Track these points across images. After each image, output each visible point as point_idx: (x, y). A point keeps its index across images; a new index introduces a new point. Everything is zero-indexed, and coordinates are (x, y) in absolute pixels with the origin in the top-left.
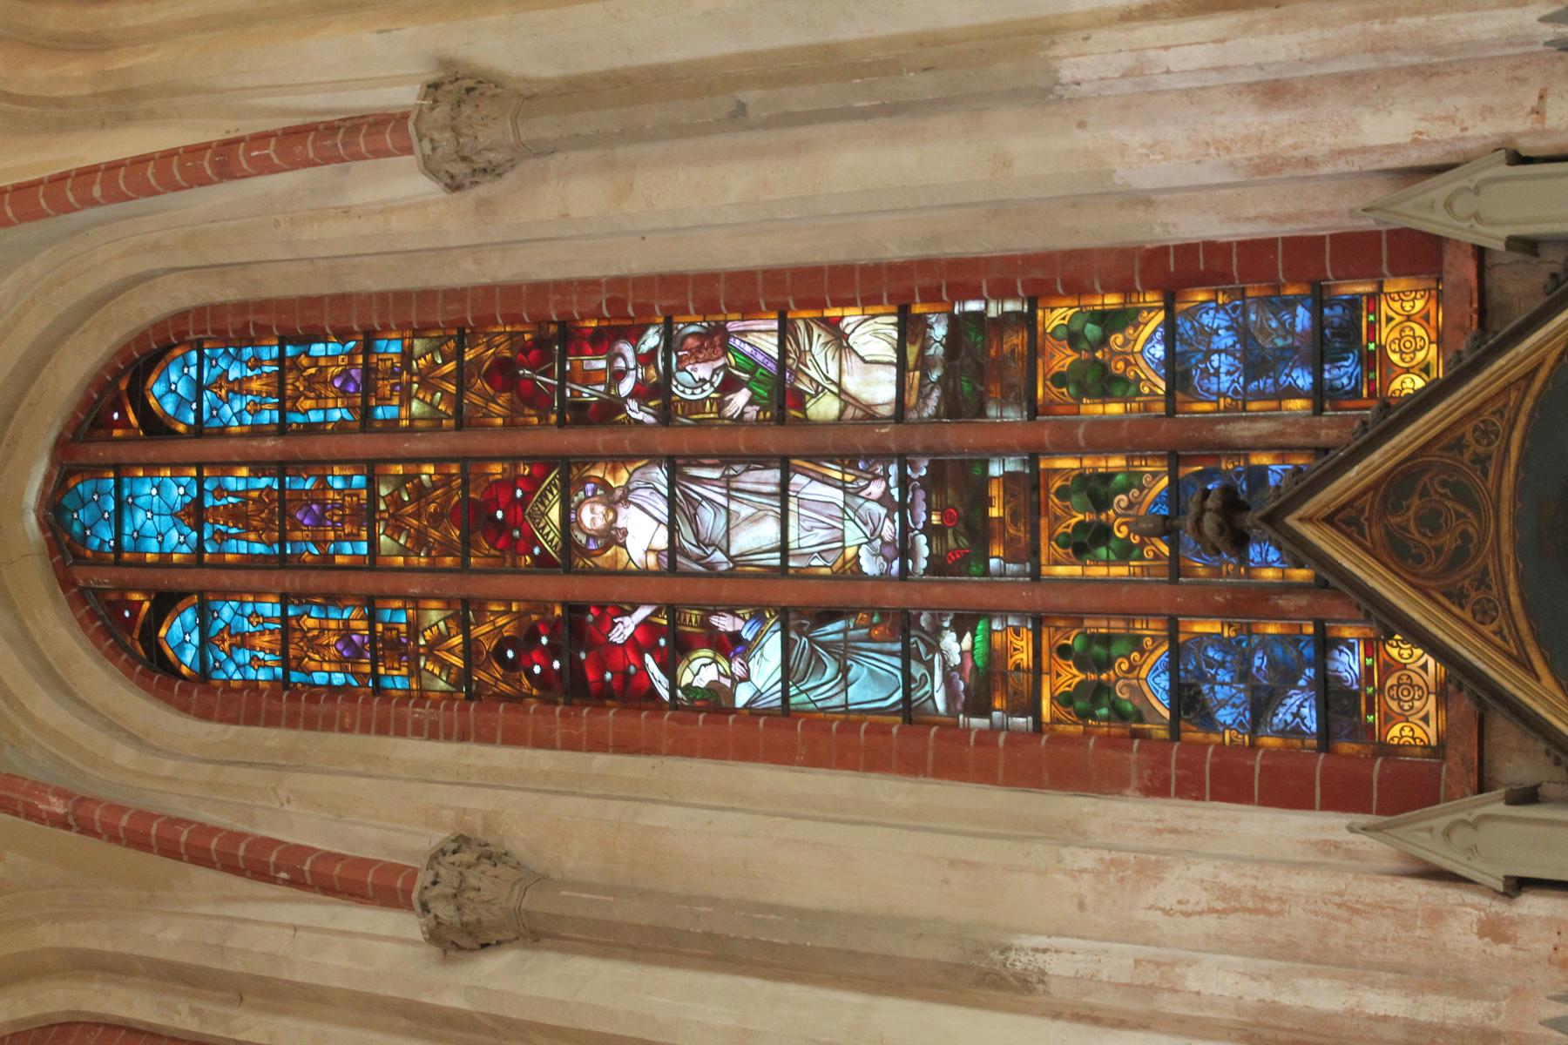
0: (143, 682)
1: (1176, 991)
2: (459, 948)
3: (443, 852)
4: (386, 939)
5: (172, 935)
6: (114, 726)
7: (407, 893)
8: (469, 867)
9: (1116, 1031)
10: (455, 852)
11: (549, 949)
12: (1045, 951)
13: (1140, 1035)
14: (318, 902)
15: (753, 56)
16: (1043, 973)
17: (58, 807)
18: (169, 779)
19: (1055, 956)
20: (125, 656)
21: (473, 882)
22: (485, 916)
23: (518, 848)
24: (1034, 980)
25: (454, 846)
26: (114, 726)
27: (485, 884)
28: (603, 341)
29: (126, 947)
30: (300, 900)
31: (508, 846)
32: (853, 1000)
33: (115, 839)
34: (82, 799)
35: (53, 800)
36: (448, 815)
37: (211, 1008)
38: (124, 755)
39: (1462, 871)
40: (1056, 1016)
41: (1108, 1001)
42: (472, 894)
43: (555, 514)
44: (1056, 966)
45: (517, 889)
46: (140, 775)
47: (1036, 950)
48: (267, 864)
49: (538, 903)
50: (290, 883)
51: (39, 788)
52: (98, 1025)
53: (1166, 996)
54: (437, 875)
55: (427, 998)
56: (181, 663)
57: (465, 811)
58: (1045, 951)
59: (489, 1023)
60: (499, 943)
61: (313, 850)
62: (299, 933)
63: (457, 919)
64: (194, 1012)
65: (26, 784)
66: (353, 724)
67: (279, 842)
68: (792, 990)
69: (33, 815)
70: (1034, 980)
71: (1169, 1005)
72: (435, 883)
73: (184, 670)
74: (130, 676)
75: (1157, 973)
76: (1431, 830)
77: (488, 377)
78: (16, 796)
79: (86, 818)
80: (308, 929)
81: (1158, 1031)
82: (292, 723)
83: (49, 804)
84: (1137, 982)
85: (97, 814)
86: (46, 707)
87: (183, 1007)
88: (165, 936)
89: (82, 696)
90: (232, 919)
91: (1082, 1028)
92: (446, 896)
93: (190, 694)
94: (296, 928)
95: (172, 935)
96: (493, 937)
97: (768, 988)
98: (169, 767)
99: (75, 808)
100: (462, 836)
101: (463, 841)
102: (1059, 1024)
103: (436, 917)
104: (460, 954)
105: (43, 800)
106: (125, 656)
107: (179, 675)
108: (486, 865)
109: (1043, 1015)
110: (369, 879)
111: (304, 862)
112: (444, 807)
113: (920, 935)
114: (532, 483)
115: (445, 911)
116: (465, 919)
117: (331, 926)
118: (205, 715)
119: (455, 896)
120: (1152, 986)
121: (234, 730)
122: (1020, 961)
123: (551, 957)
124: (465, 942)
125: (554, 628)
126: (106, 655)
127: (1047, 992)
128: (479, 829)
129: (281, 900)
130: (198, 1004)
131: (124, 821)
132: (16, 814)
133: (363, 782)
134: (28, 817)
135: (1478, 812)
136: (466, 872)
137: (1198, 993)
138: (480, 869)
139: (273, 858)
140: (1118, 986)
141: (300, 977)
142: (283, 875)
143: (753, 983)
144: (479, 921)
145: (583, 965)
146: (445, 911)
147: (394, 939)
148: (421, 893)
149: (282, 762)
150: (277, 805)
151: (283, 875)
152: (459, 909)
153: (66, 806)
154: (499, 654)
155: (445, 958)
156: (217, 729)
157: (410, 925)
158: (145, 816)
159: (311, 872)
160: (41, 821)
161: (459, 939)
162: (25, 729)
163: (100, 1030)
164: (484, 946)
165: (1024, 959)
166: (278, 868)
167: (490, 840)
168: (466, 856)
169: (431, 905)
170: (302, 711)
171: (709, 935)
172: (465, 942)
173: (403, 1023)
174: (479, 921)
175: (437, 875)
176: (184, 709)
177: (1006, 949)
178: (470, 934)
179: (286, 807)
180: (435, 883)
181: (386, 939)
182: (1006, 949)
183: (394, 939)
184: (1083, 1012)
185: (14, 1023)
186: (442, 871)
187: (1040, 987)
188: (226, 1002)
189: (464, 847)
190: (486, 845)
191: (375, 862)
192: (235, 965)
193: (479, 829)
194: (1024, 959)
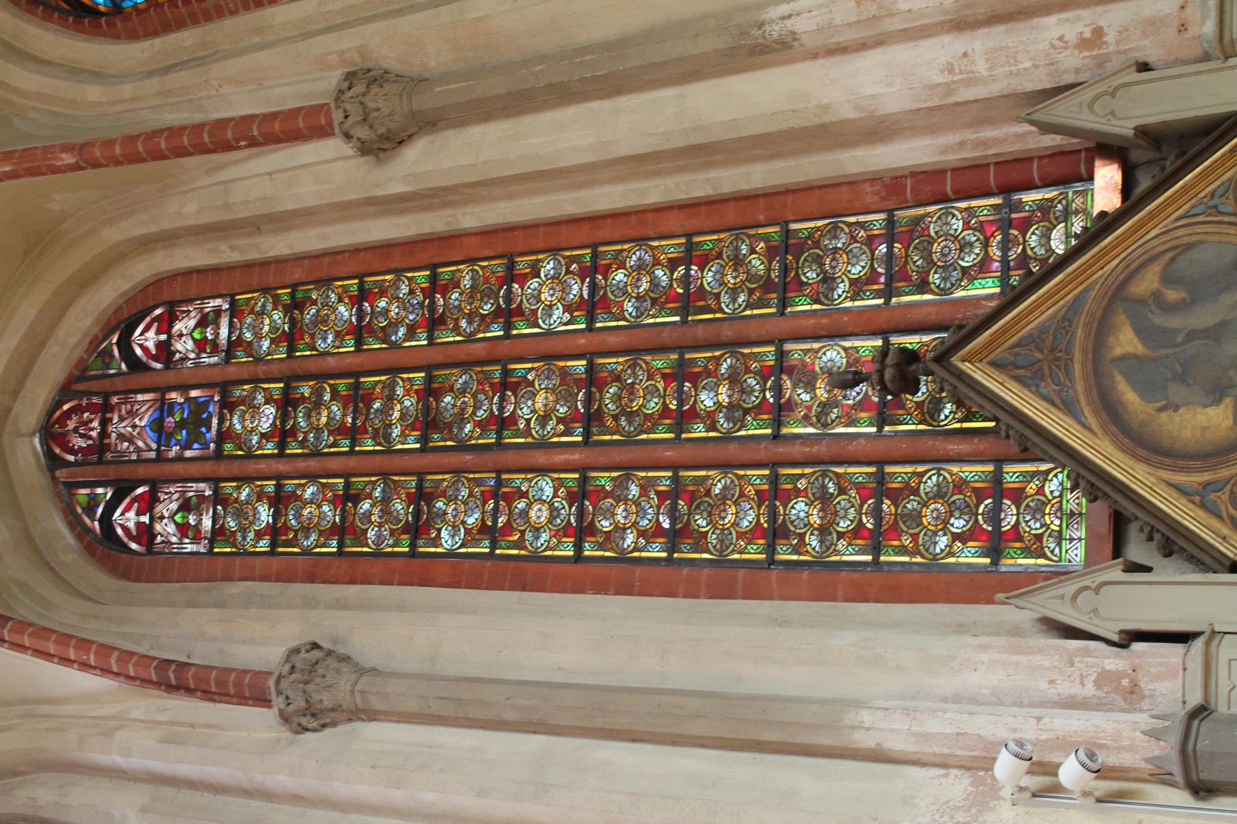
0: (78, 28)
1: (893, 15)
2: (385, 150)
3: (341, 92)
4: (333, 160)
5: (191, 208)
6: (75, 72)
7: (331, 125)
8: (364, 95)
9: (861, 53)
10: (350, 88)
11: (447, 128)
12: (789, 16)
13: (879, 51)
14: (276, 150)
15: (162, 232)
16: (793, 33)
17: (68, 159)
18: (133, 99)
19: (798, 19)
20: (56, 15)
21: (372, 105)
22: (392, 125)
23: (392, 64)
24: (789, 39)
25: (347, 84)
26: (75, 72)
27: (381, 104)
29: (166, 225)
30: (263, 153)
31: (385, 65)
32: (668, 93)
33: (118, 164)
34: (83, 146)
35: (63, 156)
36: (333, 58)
37: (242, 242)
38: (94, 92)
39: (1078, 81)
40: (815, 56)
41: (846, 36)
42: (375, 114)
44: (801, 25)
45: (404, 98)
46: (113, 103)
47: (783, 18)
48: (227, 141)
49: (425, 102)
50: (250, 146)
51: (48, 150)
52: (176, 275)
53: (888, 20)
54: (345, 111)
55: (379, 192)
56: (97, 4)
57: (342, 52)
58: (789, 16)
59: (429, 193)
60: (410, 136)
61: (253, 117)
62: (274, 176)
63: (373, 136)
64: (232, 248)
65: (39, 152)
66: (236, 6)
67: (229, 120)
68: (624, 101)
69: (55, 170)
70: (789, 39)
71: (891, 25)
72: (346, 117)
73: (102, 8)
74: (67, 27)
75: (875, 6)
76: (1062, 597)
78: (36, 164)
79: (93, 155)
80: (278, 171)
81: (891, 43)
82: (195, 21)
83: (61, 159)
84: (862, 18)
85: (98, 154)
86: (25, 79)
87: (223, 247)
88: (187, 208)
89: (45, 57)
90: (225, 182)
91: (836, 59)
92: (358, 123)
93: (114, 25)
94: (270, 174)
95: (191, 208)
96: (404, 135)
97: (607, 105)
98: (127, 90)
99: (80, 155)
100: (349, 73)
101: (351, 77)
102: (819, 62)
103: (359, 139)
104: (387, 154)
105: (56, 159)
106: (56, 15)
107: (102, 14)
108: (375, 89)
109: (805, 59)
110: (301, 125)
111: (252, 130)
112: (329, 54)
113: (697, 35)
115: (362, 133)
116: (379, 132)
117: (293, 164)
118: (133, 36)
119: (365, 119)
120: (874, 17)
121: (157, 42)
122: (774, 31)
123: (450, 134)
124: (387, 146)
126: (44, 19)
127: (802, 45)
128: (358, 60)
129: (251, 157)
130: (234, 242)
131: (118, 150)
132: (43, 174)
133: (263, 54)
134: (54, 173)
135: (1100, 578)
136: (363, 100)
137: (909, 11)
138: (372, 93)
139: (230, 136)
140: (850, 25)
141: (290, 206)
142: (243, 143)
143: (595, 105)
144: (389, 130)
145: (475, 132)
146: (362, 133)
147: (338, 159)
148: (341, 128)
149: (203, 54)
150: (214, 93)
151: (243, 143)
152: (371, 127)
153: (73, 156)
155: (380, 162)
156: (146, 44)
157: (332, 147)
158: (130, 139)
159: (261, 134)
160: (63, 172)
161: (382, 146)
162: (19, 100)
163: (179, 278)
164: (400, 143)
165: (777, 28)
166: (237, 140)
167: (371, 65)
168: (359, 89)
169: (352, 132)
170: (197, 10)
171: (550, 85)
172: (387, 146)
173: (372, 209)
174: (389, 130)
175: (345, 111)
176: (117, 37)
177: (761, 25)
178: (387, 139)
179: (221, 91)
180: (346, 117)
181: (333, 160)
182: (761, 25)
183: (338, 159)
184: (833, 47)
185: (122, 295)
186: (348, 107)
187: (796, 43)
188: (250, 234)
189: (355, 82)
190: (369, 70)
191: (301, 108)
192: (243, 213)
193: (358, 60)
194: (777, 28)
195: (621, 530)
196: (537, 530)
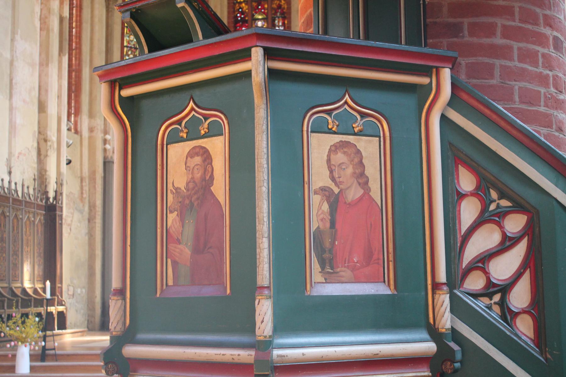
28: (284, 24)
43: (260, 17)
77: (279, 4)
114: (264, 13)
125: (244, 17)
154: (240, 8)
195: (128, 56)
196: (129, 37)
